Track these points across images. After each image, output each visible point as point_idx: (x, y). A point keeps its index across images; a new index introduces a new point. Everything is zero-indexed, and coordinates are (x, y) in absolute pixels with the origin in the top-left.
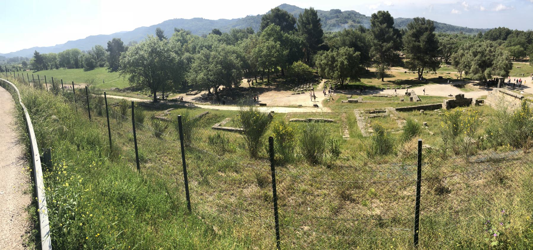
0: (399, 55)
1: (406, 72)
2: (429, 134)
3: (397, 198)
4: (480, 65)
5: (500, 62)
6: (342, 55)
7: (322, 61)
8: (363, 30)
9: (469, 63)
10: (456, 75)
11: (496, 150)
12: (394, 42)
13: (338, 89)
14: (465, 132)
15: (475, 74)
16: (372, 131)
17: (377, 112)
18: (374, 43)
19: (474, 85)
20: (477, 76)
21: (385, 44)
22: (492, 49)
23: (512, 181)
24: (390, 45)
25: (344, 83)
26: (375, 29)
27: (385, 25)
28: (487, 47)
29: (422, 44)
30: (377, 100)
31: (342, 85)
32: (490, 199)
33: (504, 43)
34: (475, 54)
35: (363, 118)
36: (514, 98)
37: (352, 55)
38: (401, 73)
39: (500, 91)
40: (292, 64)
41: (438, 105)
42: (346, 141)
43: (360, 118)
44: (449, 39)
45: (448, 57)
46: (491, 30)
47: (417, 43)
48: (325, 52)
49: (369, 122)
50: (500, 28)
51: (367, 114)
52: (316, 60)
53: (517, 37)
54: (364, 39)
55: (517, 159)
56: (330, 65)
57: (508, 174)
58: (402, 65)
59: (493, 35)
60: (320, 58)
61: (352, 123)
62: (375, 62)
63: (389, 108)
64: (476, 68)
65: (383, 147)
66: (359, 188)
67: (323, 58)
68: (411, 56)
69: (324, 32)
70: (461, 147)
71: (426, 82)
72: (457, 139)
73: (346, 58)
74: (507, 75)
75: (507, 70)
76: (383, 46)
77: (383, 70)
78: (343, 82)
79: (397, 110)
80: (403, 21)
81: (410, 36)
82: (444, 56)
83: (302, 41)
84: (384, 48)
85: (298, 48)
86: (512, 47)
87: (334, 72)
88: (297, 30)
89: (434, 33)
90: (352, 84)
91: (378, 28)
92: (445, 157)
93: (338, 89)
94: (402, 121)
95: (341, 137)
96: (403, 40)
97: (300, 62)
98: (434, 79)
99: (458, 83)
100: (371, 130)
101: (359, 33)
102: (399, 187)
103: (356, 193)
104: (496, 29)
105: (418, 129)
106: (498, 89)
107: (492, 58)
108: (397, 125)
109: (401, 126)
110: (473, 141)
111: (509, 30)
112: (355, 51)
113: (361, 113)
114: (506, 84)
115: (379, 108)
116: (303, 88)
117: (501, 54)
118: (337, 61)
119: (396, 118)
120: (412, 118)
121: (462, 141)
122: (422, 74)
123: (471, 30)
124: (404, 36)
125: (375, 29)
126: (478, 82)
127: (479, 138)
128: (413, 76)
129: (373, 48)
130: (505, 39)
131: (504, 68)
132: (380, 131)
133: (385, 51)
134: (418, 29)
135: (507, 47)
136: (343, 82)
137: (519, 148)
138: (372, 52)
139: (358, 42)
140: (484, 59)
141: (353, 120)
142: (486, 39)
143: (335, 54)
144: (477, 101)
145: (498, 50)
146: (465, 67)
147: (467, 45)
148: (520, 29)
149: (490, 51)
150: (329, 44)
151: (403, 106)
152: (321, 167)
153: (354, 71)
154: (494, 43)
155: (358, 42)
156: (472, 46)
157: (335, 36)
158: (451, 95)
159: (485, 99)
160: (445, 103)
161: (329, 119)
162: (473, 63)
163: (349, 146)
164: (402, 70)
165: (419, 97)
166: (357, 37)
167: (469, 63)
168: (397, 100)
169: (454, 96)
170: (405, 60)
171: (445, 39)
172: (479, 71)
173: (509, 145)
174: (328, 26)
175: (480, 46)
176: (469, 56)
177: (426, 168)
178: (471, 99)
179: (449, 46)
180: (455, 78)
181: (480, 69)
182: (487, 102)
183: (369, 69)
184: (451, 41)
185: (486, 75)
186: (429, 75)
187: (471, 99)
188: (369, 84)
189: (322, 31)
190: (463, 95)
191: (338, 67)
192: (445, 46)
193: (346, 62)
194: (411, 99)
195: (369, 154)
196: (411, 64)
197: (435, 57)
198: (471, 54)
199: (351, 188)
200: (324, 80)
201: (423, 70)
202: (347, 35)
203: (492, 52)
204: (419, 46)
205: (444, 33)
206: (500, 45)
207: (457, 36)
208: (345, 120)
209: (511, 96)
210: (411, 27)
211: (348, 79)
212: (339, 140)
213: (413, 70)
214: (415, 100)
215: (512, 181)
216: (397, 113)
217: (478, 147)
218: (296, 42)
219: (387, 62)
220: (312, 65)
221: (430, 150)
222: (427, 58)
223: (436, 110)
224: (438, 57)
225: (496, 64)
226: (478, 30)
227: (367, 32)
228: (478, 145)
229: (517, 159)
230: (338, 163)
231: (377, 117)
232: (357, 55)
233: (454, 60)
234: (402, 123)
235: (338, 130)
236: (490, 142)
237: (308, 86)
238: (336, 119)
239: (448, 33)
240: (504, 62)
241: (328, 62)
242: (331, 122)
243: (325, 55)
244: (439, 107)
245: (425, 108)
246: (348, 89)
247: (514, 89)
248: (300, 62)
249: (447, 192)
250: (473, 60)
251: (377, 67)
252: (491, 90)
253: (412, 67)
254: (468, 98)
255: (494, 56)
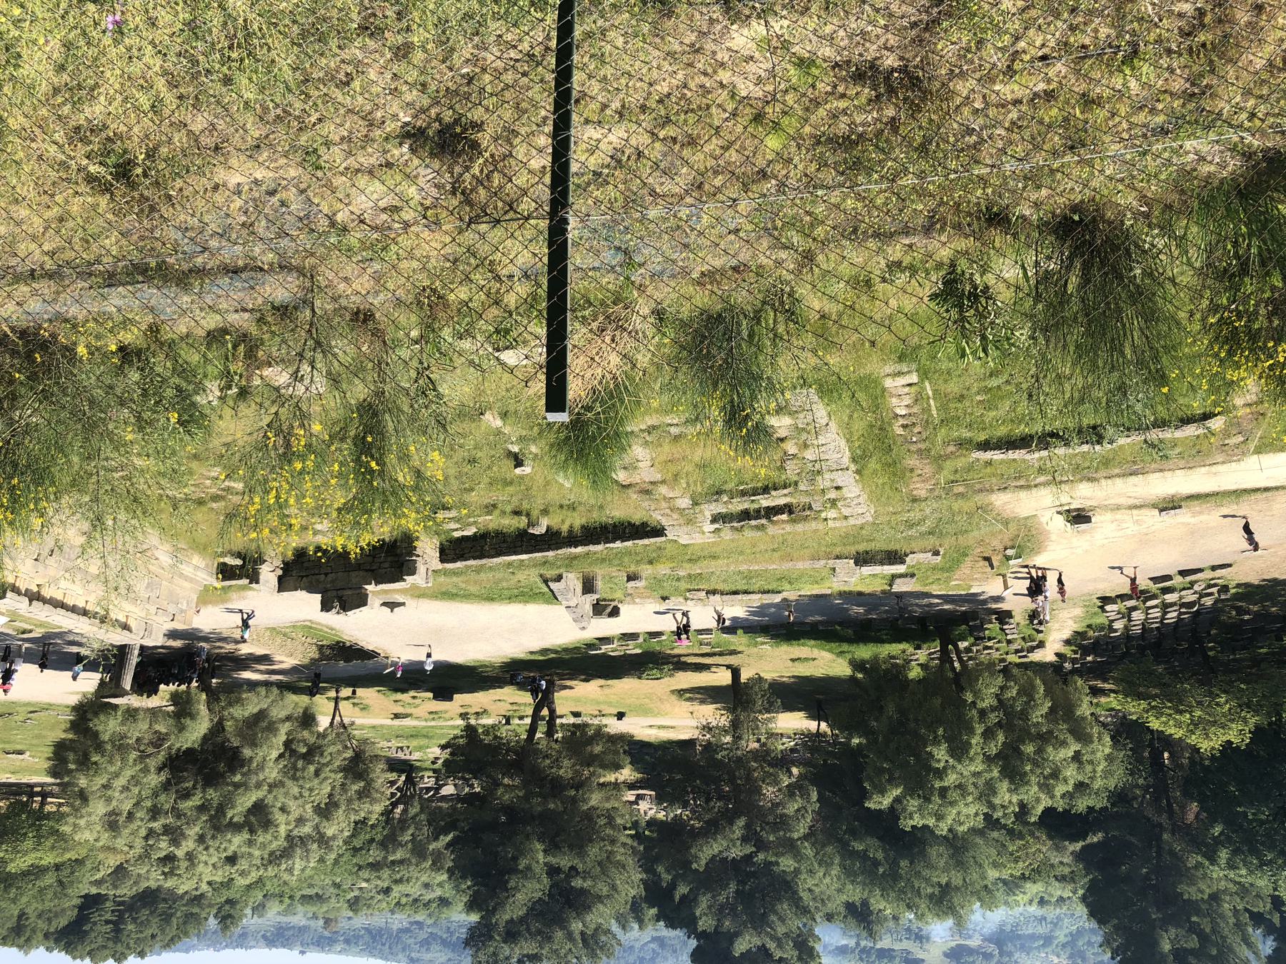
0: (659, 799)
1: (620, 716)
2: (504, 415)
3: (660, 113)
4: (234, 760)
5: (121, 784)
7: (1077, 757)
9: (292, 773)
10: (364, 708)
11: (154, 330)
13: (965, 618)
14: (317, 428)
15: (261, 715)
17: (757, 514)
18: (798, 856)
19: (265, 659)
20: (252, 705)
21: (736, 852)
22: (164, 846)
24: (706, 852)
25: (936, 646)
28: (190, 856)
29: (538, 856)
30: (758, 574)
31: (948, 642)
32: (190, 80)
33: (98, 883)
34: (259, 816)
35: (824, 482)
36: (47, 593)
38: (644, 711)
39: (125, 627)
40: (1258, 732)
41: (462, 557)
44: (397, 890)
45: (404, 798)
46: (169, 945)
47: (564, 861)
48: (1060, 805)
51: (805, 499)
52: (1109, 758)
53: (22, 915)
54: (849, 873)
56: (1025, 735)
58: (639, 751)
59: (155, 921)
60: (1086, 769)
62: (784, 761)
63: (698, 539)
64: (254, 744)
65: (722, 353)
67: (1071, 773)
68: (595, 799)
69: (1081, 910)
70: (344, 348)
71: (513, 673)
72: (359, 391)
73: (940, 774)
76: (745, 839)
77: (735, 725)
79: (658, 532)
81: (599, 898)
82: (425, 805)
83: (1213, 861)
84: (738, 833)
85: (1233, 823)
86: (49, 859)
87: (1001, 703)
88: (1257, 919)
89: (474, 918)
90: (895, 648)
92: (431, 305)
93: (972, 617)
94: (636, 479)
96: (637, 876)
97: (1205, 746)
99: (355, 666)
102: (645, 169)
104: (142, 954)
105: (558, 446)
106: (135, 640)
107: (166, 801)
108: (663, 458)
109: (638, 451)
110: (278, 376)
111: (69, 948)
112: (893, 813)
113: (833, 502)
114: (92, 666)
115: (748, 533)
116: (1165, 607)
117: (112, 823)
118: (988, 759)
119: (663, 490)
121: (334, 380)
122: (538, 709)
123: (279, 937)
124: (633, 892)
126: (247, 675)
127: (244, 393)
128: (580, 699)
129: (801, 829)
130: (91, 902)
131: (99, 747)
132: (743, 426)
133: (730, 818)
134: (559, 934)
136: (945, 656)
137: (23, 334)
138: (802, 813)
139: (880, 855)
140: (212, 794)
142: (198, 899)
143: (1006, 796)
144: (254, 578)
145: (129, 843)
146: (313, 752)
149: (174, 835)
150: (1042, 848)
151: (628, 552)
153: (891, 709)
154: (154, 878)
155: (880, 855)
156: (274, 858)
157: (1012, 885)
158: (392, 605)
160: (421, 568)
162: (272, 773)
164: (641, 728)
165: (554, 598)
166: (890, 881)
167: (292, 773)
168: (657, 582)
169: (374, 602)
170: (627, 773)
171: (414, 890)
172: (240, 733)
173: (81, 350)
174: (1061, 936)
175: (232, 860)
176: (294, 809)
177: (522, 251)
179: (398, 855)
180: (367, 694)
182: (199, 570)
183: (812, 725)
185: (203, 709)
186: (502, 708)
189: (1092, 914)
190: (326, 607)
191: (979, 729)
192: (419, 851)
193: (941, 754)
194: (588, 587)
196: (591, 760)
197: (471, 798)
198: (280, 818)
200: (1046, 655)
201: (532, 730)
202: (946, 889)
203: (167, 830)
204: (553, 847)
205: (420, 917)
206: (120, 871)
207: (354, 904)
209: (62, 606)
211: (915, 673)
213: (585, 725)
214: (572, 581)
216: (657, 517)
218: (1254, 851)
220: (1126, 732)
221: (503, 337)
222: (509, 789)
223: (470, 532)
224: (457, 798)
225: (146, 770)
226: (242, 941)
228: (250, 354)
232: (882, 792)
233: (369, 783)
236: (183, 371)
237: (1138, 616)
239: (399, 920)
240: (101, 780)
241: (1040, 751)
243: (1060, 789)
244: (453, 550)
245: (522, 542)
246: (912, 619)
248: (1208, 744)
249: (422, 131)
250: (272, 786)
251: (771, 735)
252: (173, 634)
253: (585, 743)
254: (301, 595)
255: (155, 813)
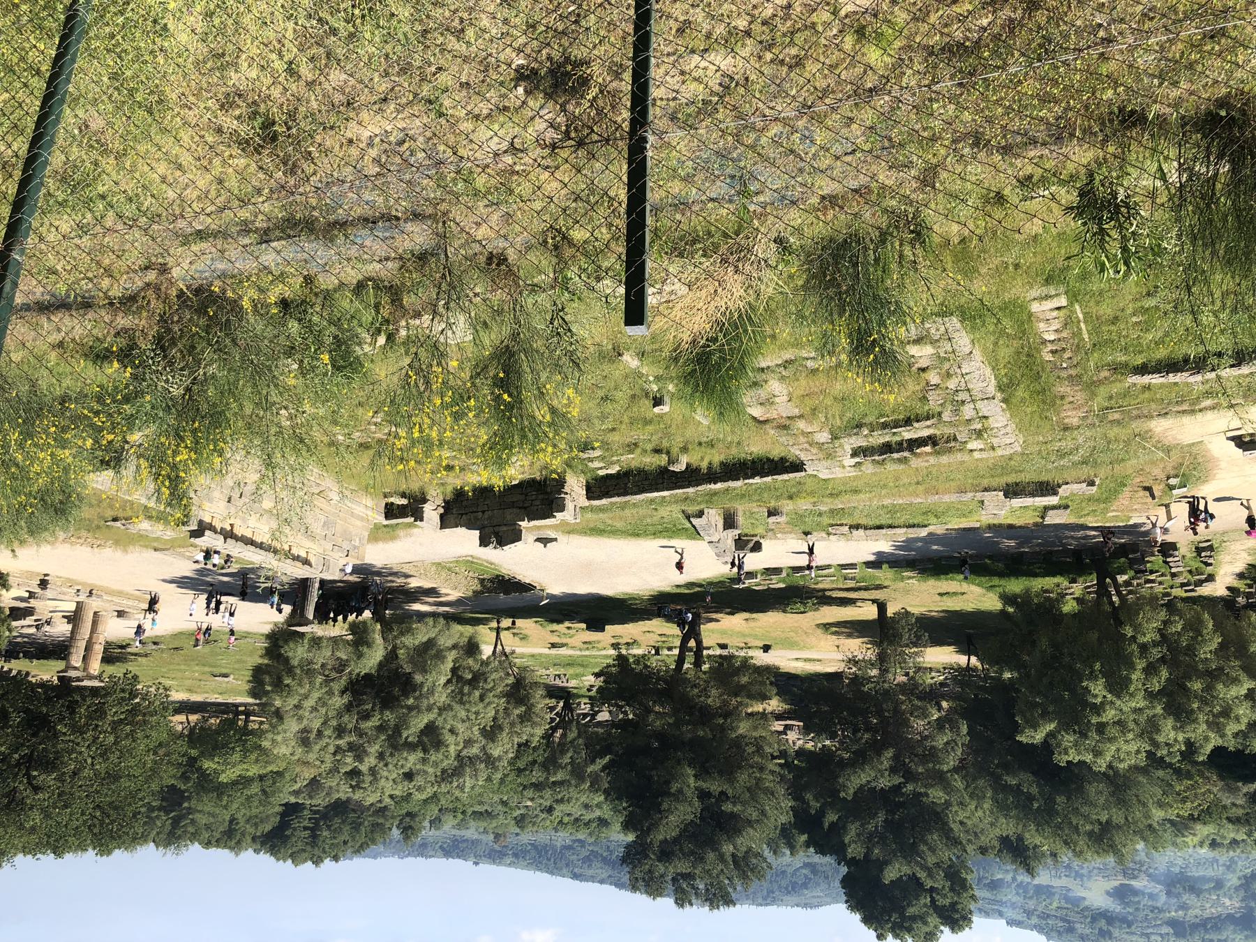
0: (806, 730)
1: (766, 648)
4: (408, 686)
5: (311, 705)
6: (1122, 727)
8: (1018, 852)
10: (524, 638)
12: (834, 793)
13: (1123, 550)
15: (430, 643)
16: (913, 350)
17: (900, 447)
19: (432, 592)
20: (422, 634)
21: (884, 782)
22: (349, 762)
23: (219, 131)
24: (855, 781)
25: (1093, 580)
26: (947, 854)
27: (891, 874)
28: (373, 771)
30: (902, 508)
33: (296, 793)
34: (431, 737)
36: (238, 531)
37: (1065, 726)
38: (789, 644)
39: (306, 562)
42: (1048, 281)
43: (985, 408)
45: (563, 722)
46: (359, 850)
47: (714, 786)
48: (1231, 745)
49: (932, 396)
50: (317, 861)
51: (948, 431)
55: (201, 235)
56: (1192, 671)
57: (242, 162)
58: (785, 683)
61: (1026, 378)
62: (933, 695)
63: (838, 473)
64: (424, 671)
65: (849, 281)
66: (954, 50)
68: (743, 728)
71: (659, 605)
73: (1098, 709)
74: (278, 640)
75: (275, 665)
76: (893, 770)
77: (882, 658)
78: (1101, 584)
79: (798, 467)
80: (792, 890)
81: (749, 823)
82: (583, 729)
84: (886, 764)
86: (254, 771)
87: (1164, 638)
89: (631, 837)
90: (1048, 582)
91: (931, 860)
95: (1073, 297)
96: (788, 803)
98: (623, 621)
100: (923, 353)
101: (1033, 838)
103: (961, 19)
104: (336, 858)
106: (315, 573)
107: (350, 721)
108: (785, 396)
115: (890, 467)
117: (304, 740)
118: (1150, 695)
119: (801, 424)
120: (722, 431)
123: (454, 849)
124: (783, 819)
125: (947, 854)
126: (417, 607)
128: (726, 632)
129: (951, 762)
130: (291, 810)
131: (290, 671)
132: (873, 353)
133: (877, 748)
134: (711, 856)
135: (279, 774)
136: (1102, 590)
138: (952, 746)
139: (1034, 790)
140: (388, 715)
141: (1020, 393)
143: (1170, 733)
144: (419, 516)
146: (478, 678)
147: (469, 782)
148: (221, 855)
149: (358, 752)
150: (1213, 788)
151: (768, 488)
152: (1176, 105)
153: (1044, 643)
155: (1034, 790)
156: (446, 776)
157: (1181, 826)
158: (545, 541)
159: (377, 527)
161: (1155, 380)
162: (441, 697)
163: (1029, 258)
164: (786, 660)
165: (696, 533)
166: (1046, 816)
168: (799, 517)
169: (528, 538)
170: (774, 705)
171: (577, 811)
172: (411, 660)
173: (246, 304)
175: (409, 776)
176: (463, 728)
178: (445, 522)
179: (560, 776)
180: (526, 625)
181: (408, 669)
182: (369, 510)
183: (962, 660)
184: (547, 798)
185: (378, 638)
186: (651, 638)
187: (445, 522)
188: (952, 584)
190: (484, 542)
191: (1140, 664)
192: (578, 773)
193: (1098, 689)
194: (729, 522)
195: (919, 234)
196: (738, 690)
197: (625, 724)
198: (450, 739)
199: (996, 37)
200: (1217, 589)
201: (680, 660)
203: (351, 747)
206: (314, 783)
207: (520, 821)
208: (1063, 389)
209: (250, 542)
210: (745, 866)
211: (1069, 606)
212: (1084, 276)
213: (732, 657)
214: (714, 517)
215: (219, 131)
216: (796, 452)
217: (395, 293)
219: (865, 697)
225: (330, 693)
226: (423, 850)
227: (991, 837)
229: (201, 235)
230: (1080, 155)
231: (896, 424)
232: (1035, 727)
234: (768, 402)
235: (1095, 331)
238: (1116, 388)
239: (563, 838)
240: (293, 701)
241: (1209, 688)
242: (1143, 370)
243: (1232, 728)
246: (1066, 551)
247: (243, 574)
250: (442, 710)
251: (919, 669)
253: (730, 671)
254: (461, 531)
255: (340, 731)
